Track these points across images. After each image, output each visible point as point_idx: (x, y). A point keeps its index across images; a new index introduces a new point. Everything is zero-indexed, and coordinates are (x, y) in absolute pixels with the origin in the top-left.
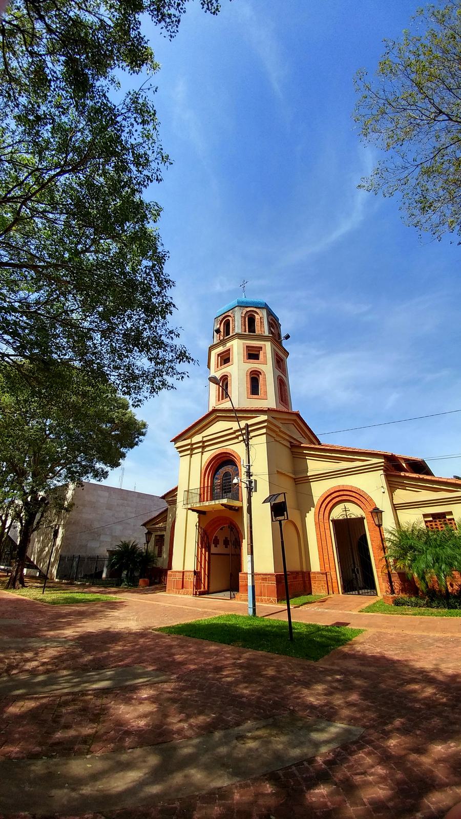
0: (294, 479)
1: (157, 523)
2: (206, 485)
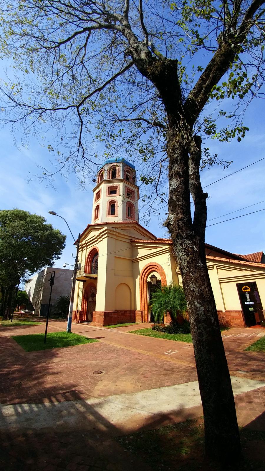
0: (132, 260)
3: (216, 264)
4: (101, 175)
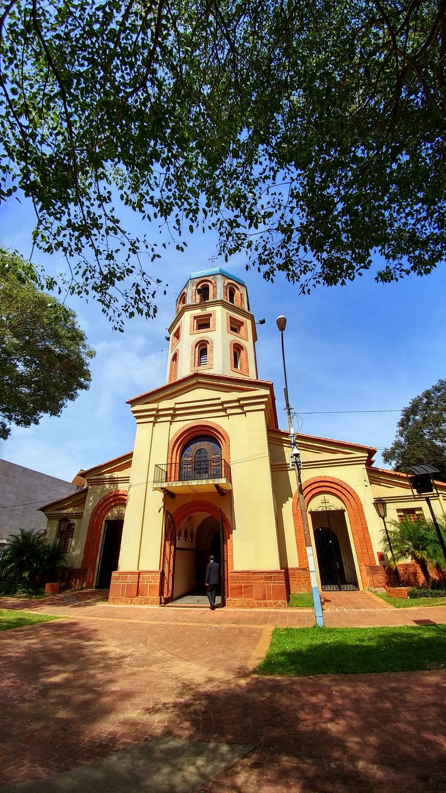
1: (65, 508)
2: (174, 462)
3: (443, 492)
4: (183, 298)
